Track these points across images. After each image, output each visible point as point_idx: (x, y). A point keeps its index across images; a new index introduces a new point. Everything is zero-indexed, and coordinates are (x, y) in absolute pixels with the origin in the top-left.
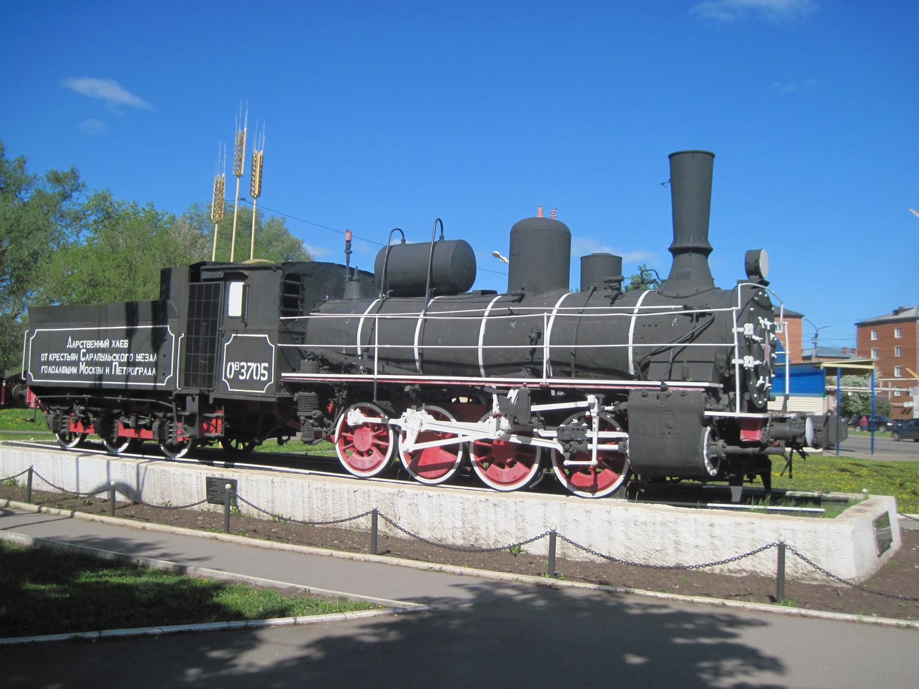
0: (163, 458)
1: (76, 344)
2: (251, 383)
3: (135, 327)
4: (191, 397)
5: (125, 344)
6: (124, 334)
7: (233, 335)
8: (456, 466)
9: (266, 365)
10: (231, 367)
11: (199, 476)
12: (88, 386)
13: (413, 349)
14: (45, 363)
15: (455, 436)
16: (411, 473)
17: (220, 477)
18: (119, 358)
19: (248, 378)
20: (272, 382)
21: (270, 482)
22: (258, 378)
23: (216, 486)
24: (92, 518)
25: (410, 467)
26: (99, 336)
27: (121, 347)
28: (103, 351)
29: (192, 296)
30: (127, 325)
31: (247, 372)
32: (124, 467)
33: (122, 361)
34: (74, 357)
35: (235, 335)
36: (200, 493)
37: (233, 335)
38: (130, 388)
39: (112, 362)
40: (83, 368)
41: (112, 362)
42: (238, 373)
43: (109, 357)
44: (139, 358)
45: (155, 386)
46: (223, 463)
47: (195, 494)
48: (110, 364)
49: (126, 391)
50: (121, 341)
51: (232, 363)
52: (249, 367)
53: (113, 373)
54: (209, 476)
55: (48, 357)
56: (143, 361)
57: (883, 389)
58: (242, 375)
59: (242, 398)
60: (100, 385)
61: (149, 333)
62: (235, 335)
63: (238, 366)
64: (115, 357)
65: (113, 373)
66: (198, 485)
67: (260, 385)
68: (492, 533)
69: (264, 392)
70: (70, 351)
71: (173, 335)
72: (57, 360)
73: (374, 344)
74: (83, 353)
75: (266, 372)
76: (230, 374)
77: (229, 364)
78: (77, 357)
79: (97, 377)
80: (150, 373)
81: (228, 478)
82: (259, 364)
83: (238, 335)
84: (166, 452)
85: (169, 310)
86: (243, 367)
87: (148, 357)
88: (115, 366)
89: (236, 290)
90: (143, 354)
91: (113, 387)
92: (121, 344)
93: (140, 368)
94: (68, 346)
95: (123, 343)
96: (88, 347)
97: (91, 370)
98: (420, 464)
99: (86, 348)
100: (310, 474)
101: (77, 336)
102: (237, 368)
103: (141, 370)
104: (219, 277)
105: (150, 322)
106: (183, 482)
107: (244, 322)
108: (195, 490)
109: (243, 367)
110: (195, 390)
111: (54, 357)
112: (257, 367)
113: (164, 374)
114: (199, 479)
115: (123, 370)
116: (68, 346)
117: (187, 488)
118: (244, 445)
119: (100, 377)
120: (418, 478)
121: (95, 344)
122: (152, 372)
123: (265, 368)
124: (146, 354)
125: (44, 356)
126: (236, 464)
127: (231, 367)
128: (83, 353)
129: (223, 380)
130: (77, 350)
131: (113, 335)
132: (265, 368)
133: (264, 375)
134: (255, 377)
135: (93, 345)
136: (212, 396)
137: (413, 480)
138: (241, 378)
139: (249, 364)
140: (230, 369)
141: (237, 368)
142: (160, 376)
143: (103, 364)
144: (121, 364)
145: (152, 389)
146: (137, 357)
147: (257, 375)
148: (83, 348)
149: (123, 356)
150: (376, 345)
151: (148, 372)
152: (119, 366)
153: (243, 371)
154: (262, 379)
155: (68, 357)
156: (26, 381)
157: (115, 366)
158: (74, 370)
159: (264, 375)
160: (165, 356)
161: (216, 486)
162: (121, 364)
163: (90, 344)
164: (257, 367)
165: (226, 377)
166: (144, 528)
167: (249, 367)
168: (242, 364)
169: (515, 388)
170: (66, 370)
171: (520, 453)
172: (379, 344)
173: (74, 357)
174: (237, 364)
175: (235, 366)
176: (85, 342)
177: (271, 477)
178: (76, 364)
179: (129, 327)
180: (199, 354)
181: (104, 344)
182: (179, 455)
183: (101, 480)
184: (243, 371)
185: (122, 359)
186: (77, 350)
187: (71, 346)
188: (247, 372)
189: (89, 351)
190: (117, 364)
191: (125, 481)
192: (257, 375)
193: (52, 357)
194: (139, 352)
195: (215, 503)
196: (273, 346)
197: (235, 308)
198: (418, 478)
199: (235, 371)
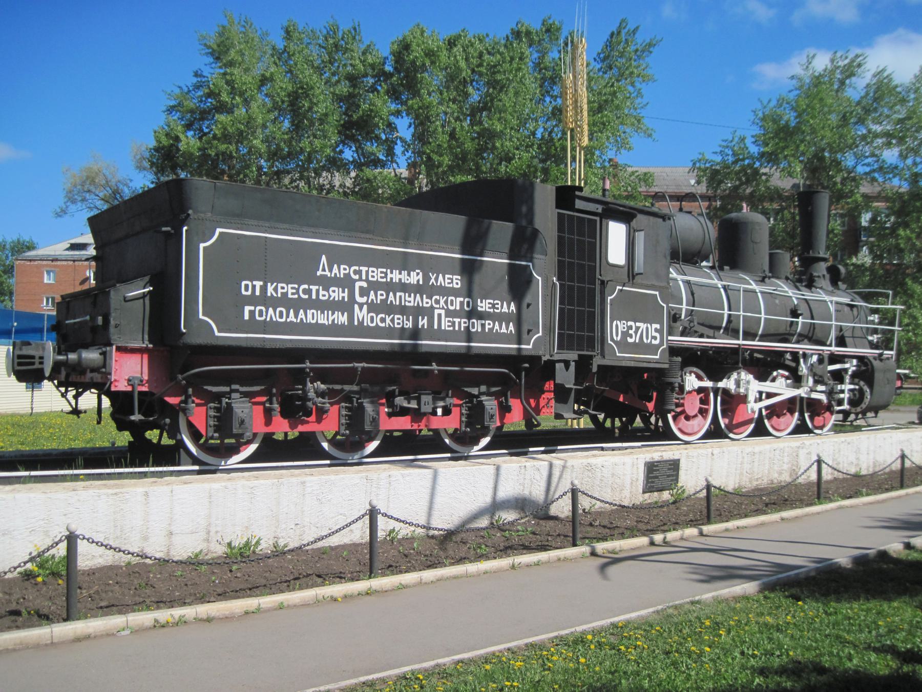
0: (328, 462)
1: (339, 271)
2: (640, 347)
3: (479, 258)
4: (562, 365)
5: (455, 281)
6: (458, 267)
7: (618, 288)
8: (754, 421)
9: (658, 326)
10: (617, 326)
11: (635, 463)
12: (387, 349)
13: (723, 314)
14: (252, 300)
15: (775, 395)
16: (726, 431)
17: (659, 459)
18: (446, 302)
19: (637, 341)
20: (217, 334)
21: (710, 455)
22: (649, 341)
23: (658, 470)
24: (724, 528)
25: (726, 426)
26: (405, 264)
27: (447, 285)
28: (417, 289)
29: (561, 229)
30: (463, 253)
31: (636, 332)
32: (523, 470)
33: (451, 308)
34: (337, 294)
35: (621, 288)
36: (634, 484)
37: (618, 288)
38: (474, 352)
39: (432, 308)
40: (361, 314)
41: (432, 308)
42: (626, 334)
43: (425, 300)
44: (484, 306)
45: (519, 350)
46: (542, 449)
47: (628, 486)
48: (429, 312)
49: (467, 357)
50: (447, 276)
51: (618, 322)
52: (638, 328)
53: (436, 327)
54: (648, 460)
55: (264, 289)
56: (492, 310)
57: (834, 349)
58: (631, 336)
59: (632, 364)
60: (519, 350)
61: (505, 269)
62: (621, 288)
63: (625, 326)
64: (437, 302)
65: (436, 327)
66: (633, 474)
67: (652, 349)
68: (845, 465)
69: (657, 357)
70: (326, 283)
71: (540, 278)
72: (290, 296)
73: (739, 312)
74: (361, 288)
75: (657, 335)
76: (617, 335)
77: (615, 323)
78: (346, 295)
79: (407, 334)
80: (504, 330)
81: (668, 459)
82: (649, 325)
83: (624, 288)
84: (454, 446)
85: (538, 246)
86: (630, 328)
87: (499, 306)
88: (440, 315)
89: (616, 232)
90: (492, 301)
91: (437, 350)
92: (447, 281)
93: (487, 322)
94: (319, 273)
95: (452, 279)
96: (370, 279)
97: (383, 320)
98: (734, 422)
99: (367, 280)
100: (643, 446)
101: (337, 257)
102: (624, 328)
103: (488, 324)
104: (595, 210)
105: (506, 255)
106: (613, 475)
107: (630, 273)
108: (628, 481)
109: (630, 328)
110: (572, 356)
111: (280, 291)
112: (647, 328)
113: (529, 331)
114: (635, 467)
115: (454, 323)
116: (319, 273)
117: (618, 481)
118: (621, 420)
119: (415, 333)
120: (731, 435)
121: (389, 276)
122: (296, 317)
123: (656, 330)
124: (496, 302)
125: (250, 287)
126: (559, 447)
127: (617, 326)
128: (361, 288)
129: (609, 342)
130: (346, 283)
131: (442, 266)
132: (656, 330)
133: (655, 338)
134: (645, 340)
135: (386, 276)
136: (597, 362)
137: (727, 437)
138: (630, 340)
139: (638, 324)
140: (616, 329)
141: (624, 328)
142: (525, 336)
143: (418, 311)
144: (449, 314)
145: (463, 351)
146: (479, 304)
147: (647, 338)
148: (360, 279)
149: (452, 301)
150: (763, 316)
151: (501, 328)
152: (446, 316)
153: (631, 332)
154: (654, 342)
155: (321, 292)
156: (184, 334)
157: (440, 315)
158: (342, 319)
159: (655, 338)
160: (529, 305)
161: (658, 470)
162: (449, 314)
163: (376, 274)
164: (647, 328)
165: (612, 339)
166: (782, 519)
167: (638, 328)
168: (630, 323)
169: (815, 354)
170: (323, 319)
171: (61, 357)
172: (765, 314)
173: (337, 294)
174: (624, 324)
175: (621, 325)
176: (364, 269)
177: (710, 450)
178: (346, 306)
179: (479, 258)
180: (896, 328)
181: (415, 278)
182: (476, 448)
183: (484, 499)
184: (631, 332)
185: (452, 305)
186: (346, 283)
187: (327, 273)
188: (636, 332)
189: (374, 286)
190: (443, 312)
191: (526, 492)
192: (647, 338)
193: (276, 289)
194: (484, 297)
195: (658, 491)
196: (665, 305)
197: (616, 253)
198: (731, 435)
199: (622, 332)
